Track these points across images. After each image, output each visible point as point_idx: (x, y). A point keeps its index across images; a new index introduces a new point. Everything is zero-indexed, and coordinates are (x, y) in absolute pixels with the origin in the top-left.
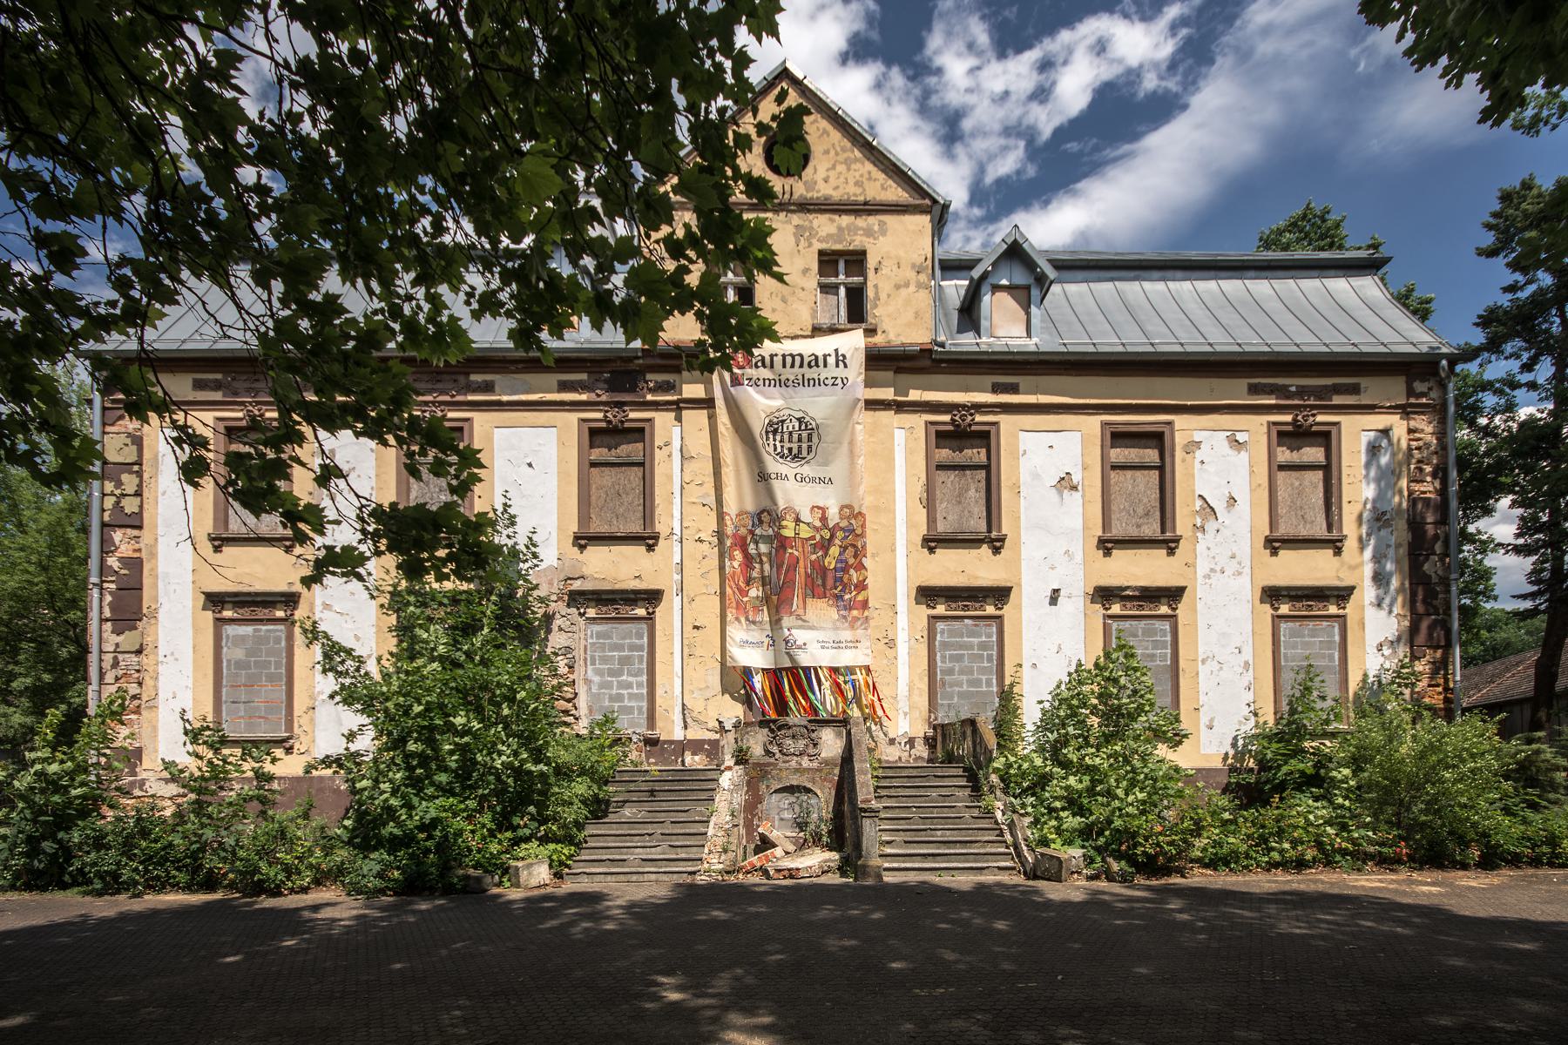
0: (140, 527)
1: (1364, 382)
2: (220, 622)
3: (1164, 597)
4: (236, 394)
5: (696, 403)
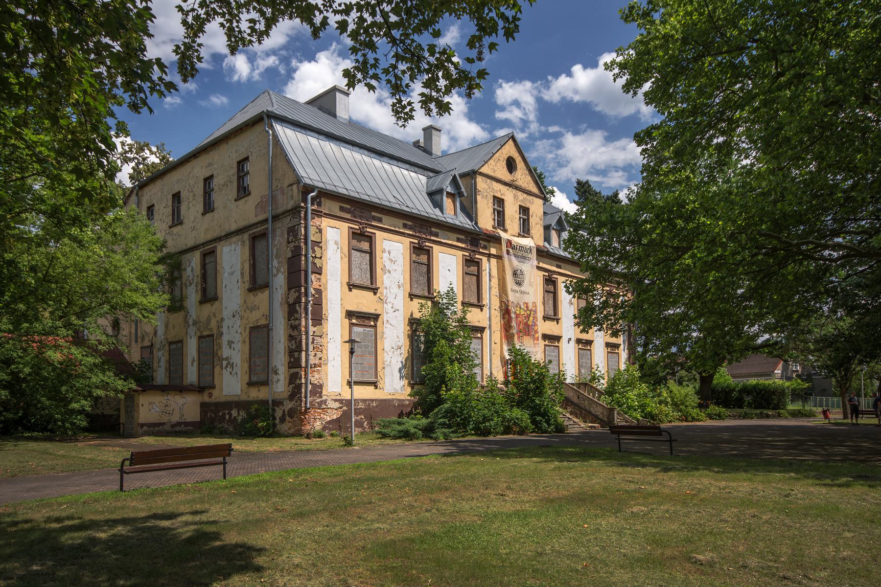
0: (320, 274)
1: (385, 218)
2: (352, 325)
3: (589, 343)
4: (355, 217)
5: (495, 256)
